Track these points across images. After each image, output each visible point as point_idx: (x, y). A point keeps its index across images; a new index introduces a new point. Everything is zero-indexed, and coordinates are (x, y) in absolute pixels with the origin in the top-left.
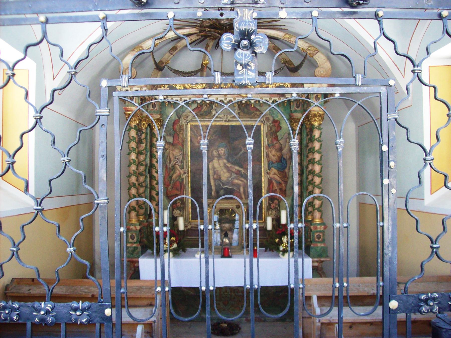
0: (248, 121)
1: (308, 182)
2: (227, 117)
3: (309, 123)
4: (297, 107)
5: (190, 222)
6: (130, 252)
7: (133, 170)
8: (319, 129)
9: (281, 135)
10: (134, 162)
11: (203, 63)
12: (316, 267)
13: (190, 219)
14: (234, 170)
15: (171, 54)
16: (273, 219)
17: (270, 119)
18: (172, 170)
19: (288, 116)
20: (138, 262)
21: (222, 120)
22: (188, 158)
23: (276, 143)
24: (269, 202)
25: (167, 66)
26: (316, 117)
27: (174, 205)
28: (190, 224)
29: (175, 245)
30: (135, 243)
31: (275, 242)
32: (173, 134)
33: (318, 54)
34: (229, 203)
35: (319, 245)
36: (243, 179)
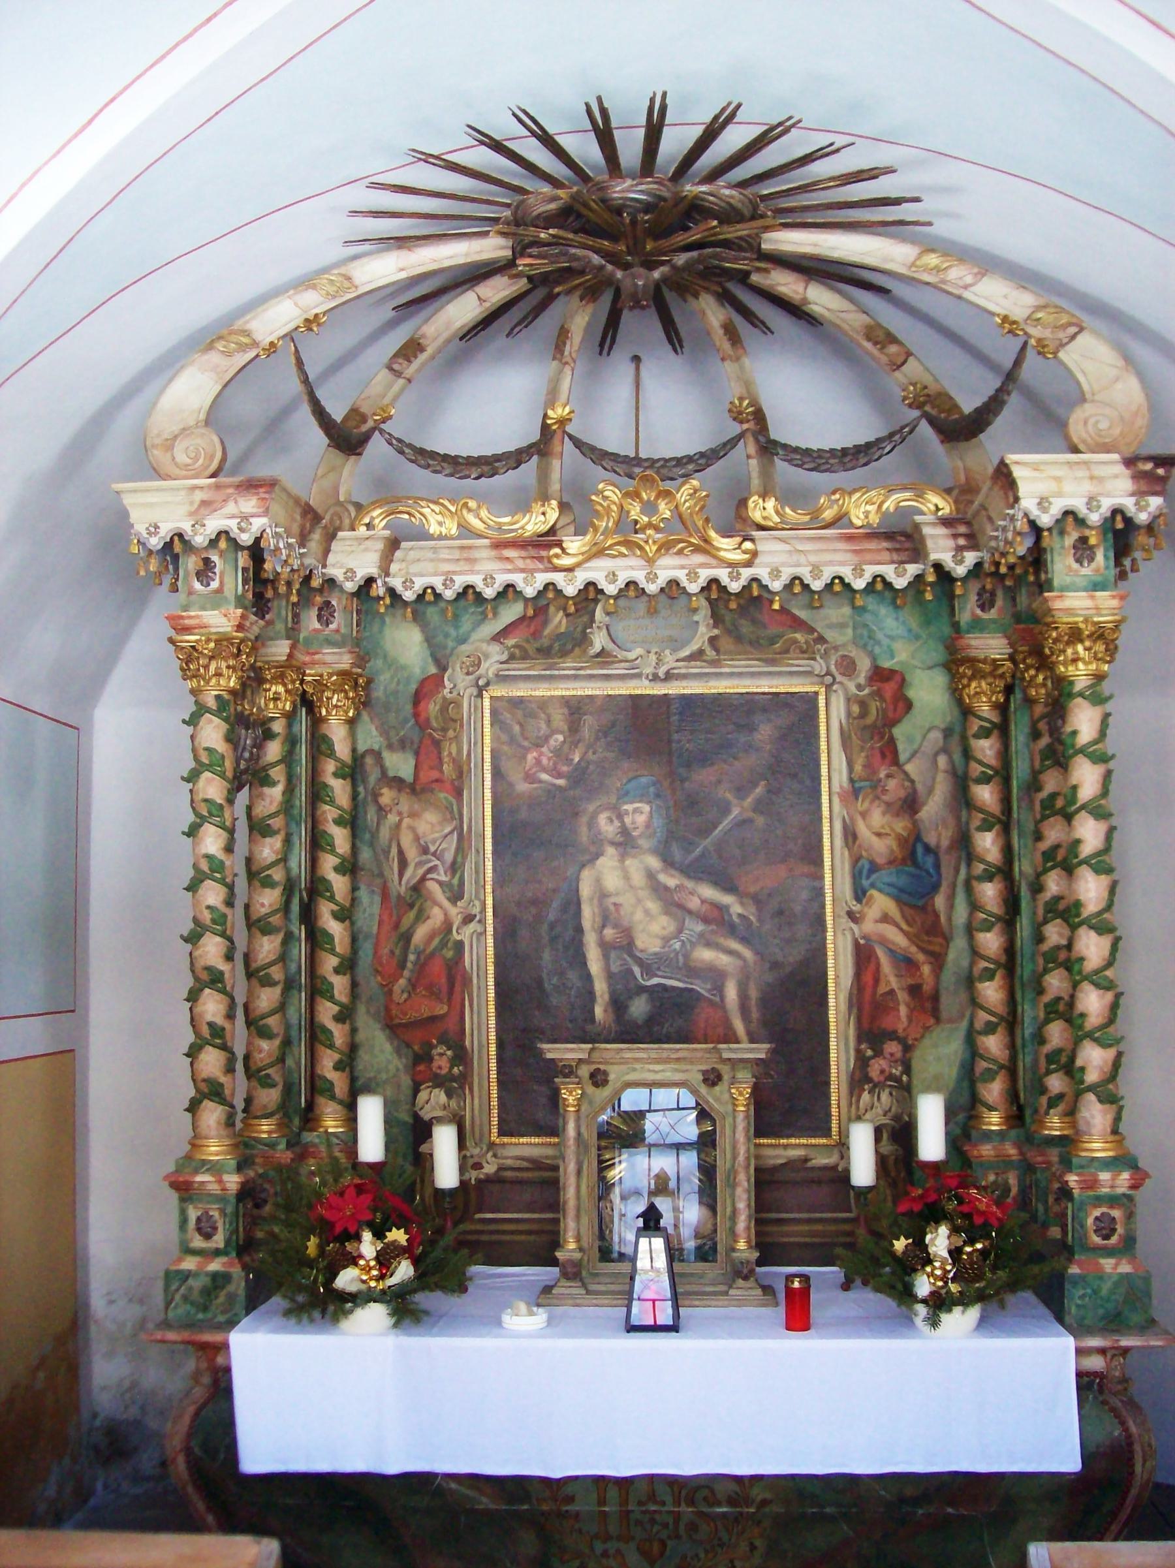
0: (760, 674)
1: (1044, 954)
2: (659, 661)
3: (1041, 677)
4: (982, 607)
5: (492, 1145)
6: (196, 1295)
7: (208, 907)
8: (1097, 698)
9: (910, 740)
10: (213, 871)
11: (545, 416)
12: (1096, 1374)
13: (495, 1130)
14: (694, 903)
15: (398, 374)
16: (878, 1132)
17: (858, 663)
18: (411, 906)
19: (941, 648)
20: (225, 1347)
21: (638, 676)
22: (480, 852)
23: (888, 776)
24: (858, 1051)
25: (382, 432)
26: (1081, 641)
27: (421, 1068)
28: (495, 1156)
29: (404, 1270)
30: (217, 1253)
31: (892, 1254)
32: (416, 740)
33: (1084, 340)
34: (667, 1061)
35: (1107, 1263)
36: (735, 945)
